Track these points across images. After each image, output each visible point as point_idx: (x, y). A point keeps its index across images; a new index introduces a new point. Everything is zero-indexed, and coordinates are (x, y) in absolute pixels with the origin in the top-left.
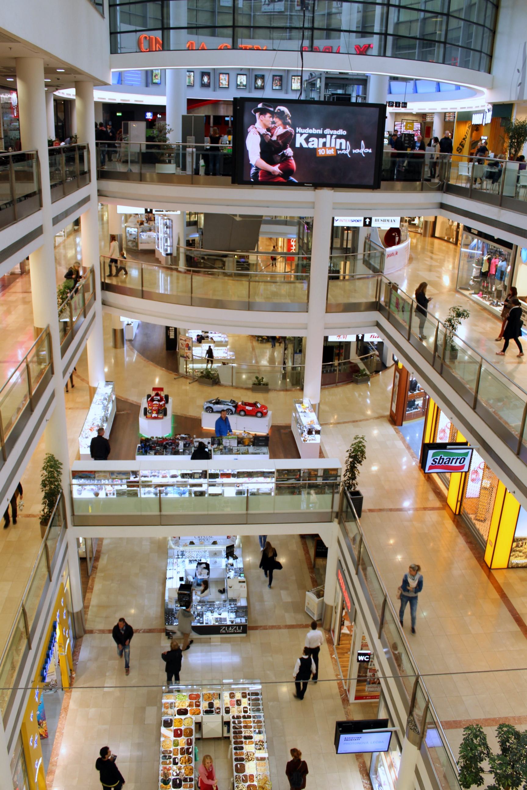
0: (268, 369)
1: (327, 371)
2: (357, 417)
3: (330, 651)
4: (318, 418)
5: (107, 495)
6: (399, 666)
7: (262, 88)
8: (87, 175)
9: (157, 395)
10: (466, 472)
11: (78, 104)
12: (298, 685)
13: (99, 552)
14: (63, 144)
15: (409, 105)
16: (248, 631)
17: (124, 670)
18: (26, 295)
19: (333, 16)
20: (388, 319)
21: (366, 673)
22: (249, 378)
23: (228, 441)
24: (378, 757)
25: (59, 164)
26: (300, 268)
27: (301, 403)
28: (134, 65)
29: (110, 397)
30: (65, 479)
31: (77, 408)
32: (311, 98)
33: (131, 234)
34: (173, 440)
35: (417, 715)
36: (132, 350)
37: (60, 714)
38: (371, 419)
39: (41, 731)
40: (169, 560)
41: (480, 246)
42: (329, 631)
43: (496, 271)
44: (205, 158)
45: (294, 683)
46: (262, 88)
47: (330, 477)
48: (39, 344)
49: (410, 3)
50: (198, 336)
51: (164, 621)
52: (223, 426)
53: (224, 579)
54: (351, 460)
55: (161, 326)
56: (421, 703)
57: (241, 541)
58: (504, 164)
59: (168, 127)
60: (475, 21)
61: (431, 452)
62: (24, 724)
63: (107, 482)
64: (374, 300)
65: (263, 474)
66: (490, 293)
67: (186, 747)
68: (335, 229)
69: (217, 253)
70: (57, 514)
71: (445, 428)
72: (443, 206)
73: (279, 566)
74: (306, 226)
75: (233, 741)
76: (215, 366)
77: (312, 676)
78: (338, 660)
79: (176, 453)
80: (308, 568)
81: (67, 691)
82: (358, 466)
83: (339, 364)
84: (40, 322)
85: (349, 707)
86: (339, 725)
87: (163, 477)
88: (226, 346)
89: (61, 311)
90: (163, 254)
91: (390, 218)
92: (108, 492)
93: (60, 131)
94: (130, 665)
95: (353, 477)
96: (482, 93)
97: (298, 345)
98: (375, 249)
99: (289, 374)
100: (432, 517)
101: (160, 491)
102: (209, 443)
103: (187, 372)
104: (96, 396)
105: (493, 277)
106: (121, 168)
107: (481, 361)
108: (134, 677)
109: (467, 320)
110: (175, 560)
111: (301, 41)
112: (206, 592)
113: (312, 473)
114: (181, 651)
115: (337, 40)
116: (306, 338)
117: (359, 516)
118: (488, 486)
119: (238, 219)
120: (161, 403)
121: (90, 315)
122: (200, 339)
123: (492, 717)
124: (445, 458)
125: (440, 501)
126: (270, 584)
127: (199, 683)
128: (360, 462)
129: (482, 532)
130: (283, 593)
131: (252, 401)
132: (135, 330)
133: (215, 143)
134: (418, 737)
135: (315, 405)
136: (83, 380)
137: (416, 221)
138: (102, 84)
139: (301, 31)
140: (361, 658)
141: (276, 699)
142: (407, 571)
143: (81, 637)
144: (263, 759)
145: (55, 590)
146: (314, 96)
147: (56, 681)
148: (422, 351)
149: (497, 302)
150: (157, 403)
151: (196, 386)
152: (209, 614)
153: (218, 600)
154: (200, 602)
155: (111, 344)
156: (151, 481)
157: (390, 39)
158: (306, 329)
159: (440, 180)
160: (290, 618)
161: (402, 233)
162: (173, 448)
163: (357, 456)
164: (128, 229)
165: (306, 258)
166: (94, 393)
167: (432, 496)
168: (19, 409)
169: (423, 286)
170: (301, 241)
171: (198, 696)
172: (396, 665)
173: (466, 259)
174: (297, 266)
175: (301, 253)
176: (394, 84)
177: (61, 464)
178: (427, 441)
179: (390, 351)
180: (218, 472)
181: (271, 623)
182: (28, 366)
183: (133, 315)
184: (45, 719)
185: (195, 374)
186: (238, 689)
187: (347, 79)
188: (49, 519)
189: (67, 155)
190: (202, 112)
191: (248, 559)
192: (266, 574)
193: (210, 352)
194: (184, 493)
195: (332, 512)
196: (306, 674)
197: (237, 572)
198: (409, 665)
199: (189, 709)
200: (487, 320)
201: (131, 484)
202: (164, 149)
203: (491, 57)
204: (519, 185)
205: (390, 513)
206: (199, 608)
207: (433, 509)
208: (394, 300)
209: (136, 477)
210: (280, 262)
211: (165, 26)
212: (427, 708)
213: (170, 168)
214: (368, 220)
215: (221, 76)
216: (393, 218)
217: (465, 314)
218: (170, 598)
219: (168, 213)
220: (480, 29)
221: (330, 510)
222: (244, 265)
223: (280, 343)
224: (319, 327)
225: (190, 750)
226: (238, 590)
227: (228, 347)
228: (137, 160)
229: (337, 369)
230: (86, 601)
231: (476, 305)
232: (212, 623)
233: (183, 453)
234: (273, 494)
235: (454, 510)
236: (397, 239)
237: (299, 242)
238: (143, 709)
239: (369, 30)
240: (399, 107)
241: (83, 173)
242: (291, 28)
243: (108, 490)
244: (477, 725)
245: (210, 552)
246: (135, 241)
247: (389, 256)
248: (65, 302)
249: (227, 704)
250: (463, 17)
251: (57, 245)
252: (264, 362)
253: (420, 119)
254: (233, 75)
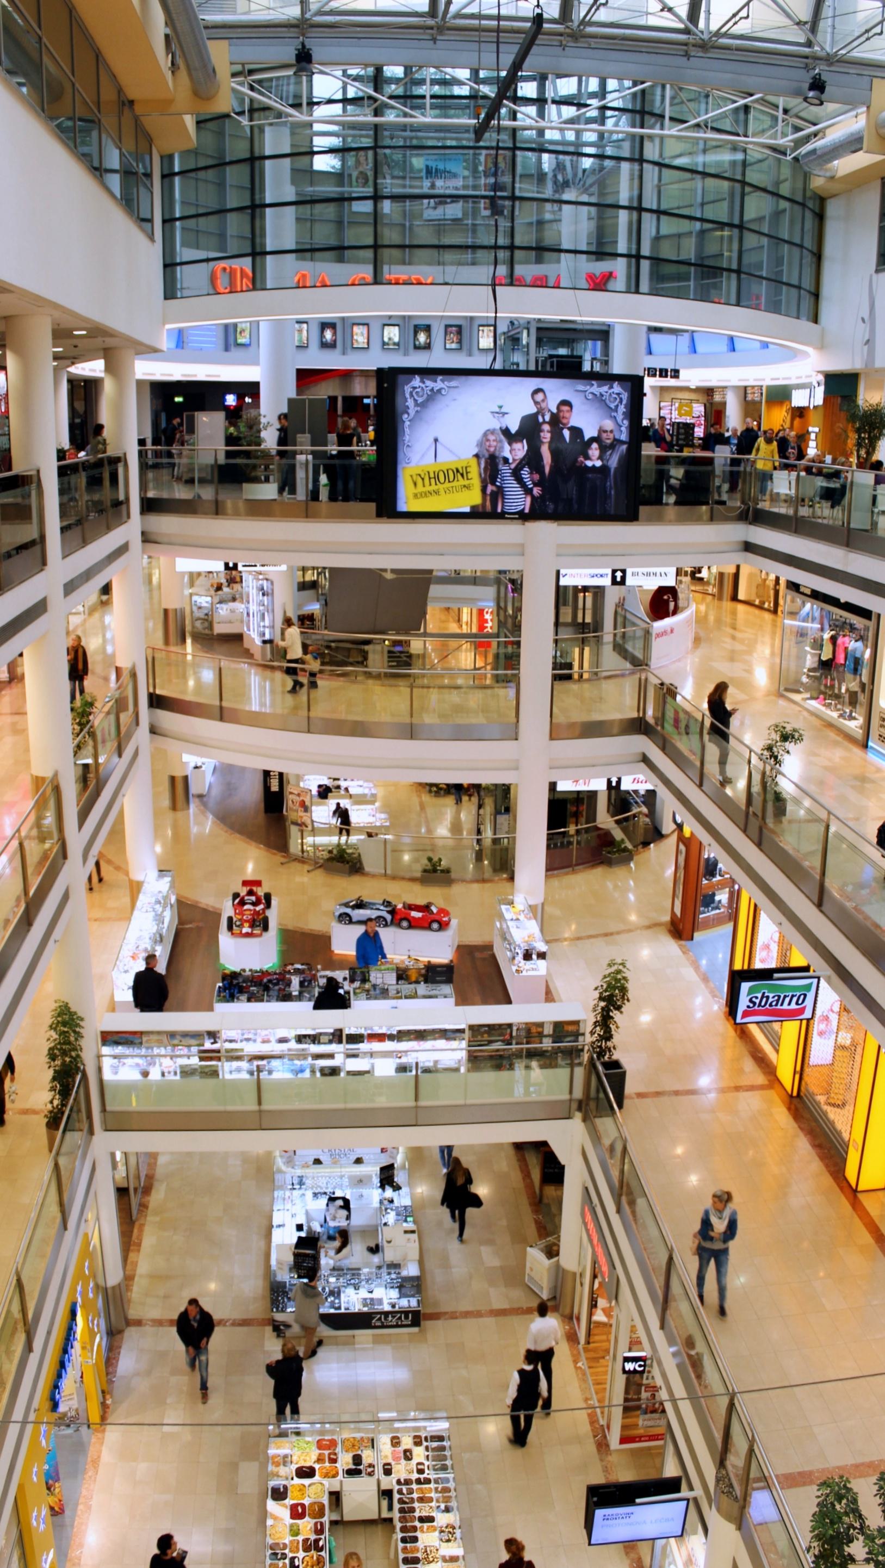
0: (450, 843)
1: (555, 845)
2: (613, 927)
3: (573, 1355)
4: (542, 930)
5: (163, 1074)
6: (699, 1377)
7: (428, 347)
8: (124, 507)
9: (251, 893)
10: (808, 1020)
11: (108, 387)
12: (515, 1420)
13: (150, 1178)
14: (82, 454)
15: (682, 373)
16: (422, 1323)
17: (199, 1393)
18: (17, 718)
19: (547, 226)
20: (663, 749)
21: (639, 1395)
22: (416, 860)
23: (379, 975)
24: (664, 1548)
25: (76, 489)
26: (502, 660)
27: (511, 903)
28: (203, 316)
29: (166, 898)
30: (89, 1046)
31: (109, 919)
32: (513, 364)
33: (200, 608)
34: (280, 974)
35: (734, 1466)
36: (203, 813)
37: (85, 1471)
38: (637, 929)
39: (52, 1500)
40: (276, 1193)
41: (817, 614)
42: (571, 1318)
43: (846, 659)
44: (329, 471)
45: (508, 1418)
46: (428, 347)
47: (566, 1036)
48: (40, 806)
49: (676, 205)
50: (320, 786)
51: (269, 1305)
52: (370, 948)
53: (377, 1226)
54: (603, 1004)
55: (255, 770)
56: (740, 1444)
57: (407, 1158)
58: (849, 475)
59: (263, 420)
60: (786, 238)
61: (745, 986)
62: (21, 1487)
63: (163, 1051)
64: (635, 715)
65: (444, 1034)
66: (838, 697)
67: (313, 1537)
68: (561, 590)
69: (355, 636)
70: (75, 1109)
71: (769, 943)
72: (749, 547)
73: (476, 1202)
74: (510, 585)
75: (398, 1525)
76: (354, 839)
77: (540, 1402)
78: (588, 1371)
79: (286, 997)
80: (531, 1204)
81: (96, 1430)
82: (615, 1014)
83: (578, 832)
84: (41, 767)
85: (610, 1458)
86: (593, 1491)
87: (264, 1042)
88: (373, 803)
89: (79, 747)
90: (258, 642)
91: (658, 570)
92: (166, 1070)
93: (77, 432)
94: (209, 1384)
95: (608, 1036)
96: (806, 354)
97: (502, 799)
98: (634, 624)
99: (487, 852)
100: (752, 1102)
101: (258, 1066)
102: (345, 979)
103: (303, 851)
104: (141, 897)
105: (841, 669)
106: (181, 493)
107: (829, 819)
108: (217, 1407)
109: (800, 746)
110: (288, 1193)
111: (492, 268)
112: (345, 1251)
113: (534, 1030)
114: (301, 1360)
115: (556, 266)
116: (517, 785)
117: (620, 1106)
118: (848, 1042)
119: (389, 576)
120: (258, 908)
121: (128, 752)
122: (324, 792)
123: (866, 1460)
124: (771, 995)
125: (765, 1073)
126: (461, 1234)
127: (334, 1418)
128: (618, 1008)
129: (839, 1126)
130: (486, 1251)
131: (421, 902)
132: (209, 778)
133: (349, 442)
134: (736, 1506)
135: (536, 906)
136: (118, 868)
137: (704, 574)
138: (150, 351)
139: (493, 252)
140: (630, 1366)
141: (475, 1446)
142: (708, 1203)
143: (121, 1332)
144: (454, 1559)
145: (71, 1252)
146: (518, 359)
147: (77, 1410)
148: (725, 805)
149: (851, 712)
150: (251, 907)
151: (319, 875)
152: (350, 1291)
153: (367, 1265)
154: (334, 1269)
155: (166, 802)
156: (242, 1050)
157: (645, 265)
158: (517, 769)
159: (743, 502)
160: (499, 1298)
161: (680, 595)
162: (280, 990)
163: (613, 996)
164: (195, 598)
165: (512, 643)
166: (139, 891)
167: (749, 1065)
168: (7, 922)
169: (720, 690)
170: (502, 613)
171: (333, 1443)
172: (693, 1376)
173: (793, 638)
174: (497, 656)
175: (502, 634)
176: (654, 337)
177: (82, 1019)
178: (738, 966)
179: (668, 806)
180: (362, 1031)
181: (465, 1306)
182: (21, 845)
183: (205, 751)
184: (58, 1480)
185: (318, 854)
186: (407, 1430)
187: (575, 330)
188: (61, 1119)
189: (91, 479)
190: (323, 391)
191: (419, 1190)
192: (453, 1216)
193: (342, 814)
194: (302, 1071)
195: (571, 1100)
196: (530, 1399)
197: (401, 1215)
198: (717, 1376)
199: (317, 1466)
200: (836, 744)
201: (206, 1055)
202: (257, 458)
203: (816, 295)
204: (876, 510)
205: (674, 1098)
206: (332, 1280)
207: (752, 1088)
208: (670, 714)
209: (215, 1042)
210: (466, 651)
211: (258, 250)
212: (751, 1451)
213: (268, 491)
214: (619, 574)
215: (356, 329)
216: (663, 570)
217: (796, 735)
218: (279, 1262)
219: (265, 568)
220: (796, 251)
221: (567, 1097)
222: (401, 659)
223: (470, 796)
224: (538, 766)
225: (321, 1543)
226: (402, 1247)
227: (377, 804)
228: (209, 478)
229: (574, 840)
230: (128, 1267)
231: (814, 718)
232: (357, 1307)
233: (300, 998)
234: (463, 1070)
235: (789, 1089)
236: (672, 605)
237: (498, 615)
238: (234, 1466)
239: (608, 249)
240: (666, 376)
241: (117, 504)
242: (474, 247)
243: (166, 1065)
244: (841, 1477)
245: (350, 1178)
246: (208, 620)
247: (658, 635)
248: (86, 730)
249: (386, 1457)
250: (766, 231)
251: (71, 628)
252: (443, 831)
253: (703, 398)
254: (375, 328)
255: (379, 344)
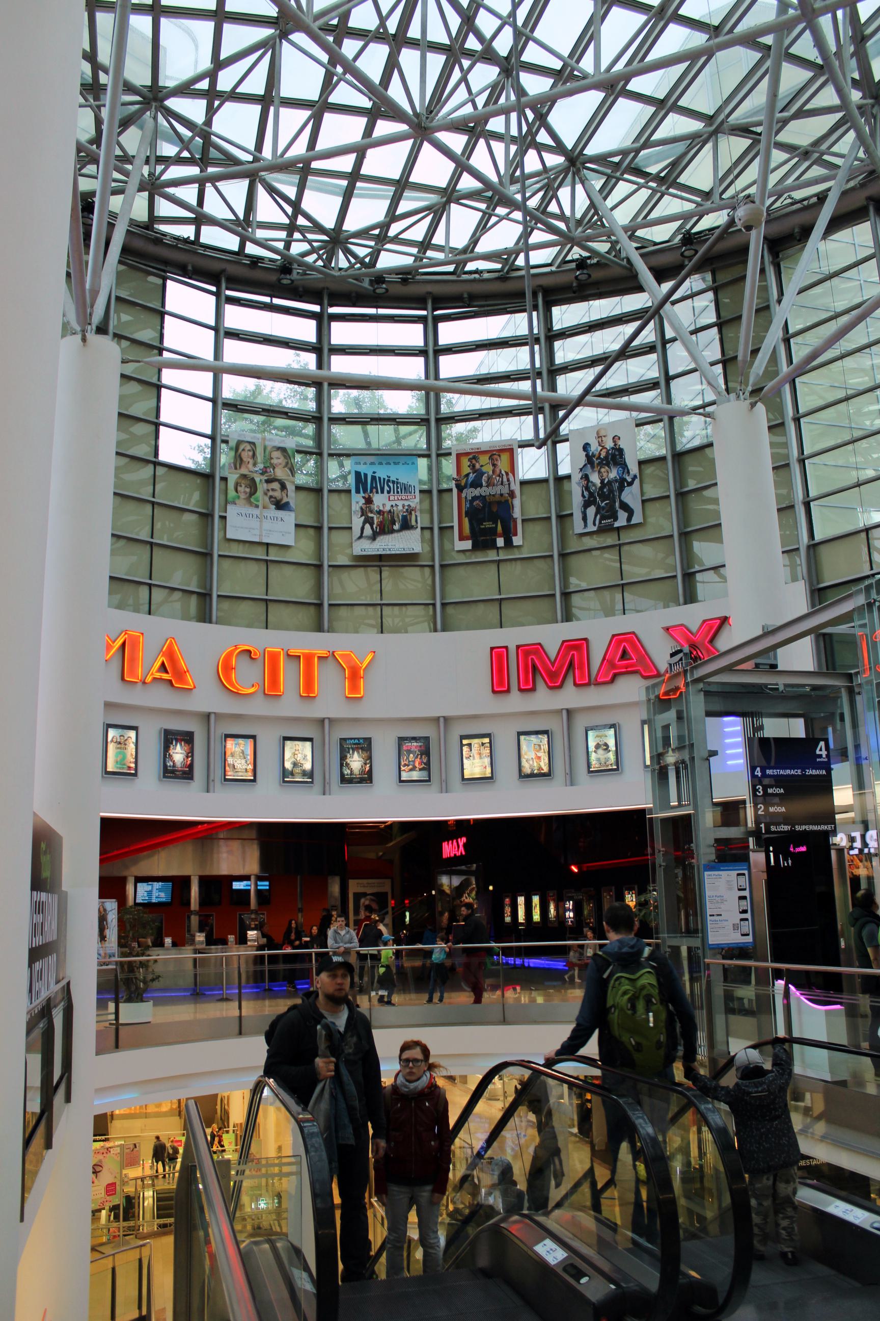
7: (367, 778)
46: (367, 778)
163: (712, 364)
215: (230, 744)
255: (276, 774)
